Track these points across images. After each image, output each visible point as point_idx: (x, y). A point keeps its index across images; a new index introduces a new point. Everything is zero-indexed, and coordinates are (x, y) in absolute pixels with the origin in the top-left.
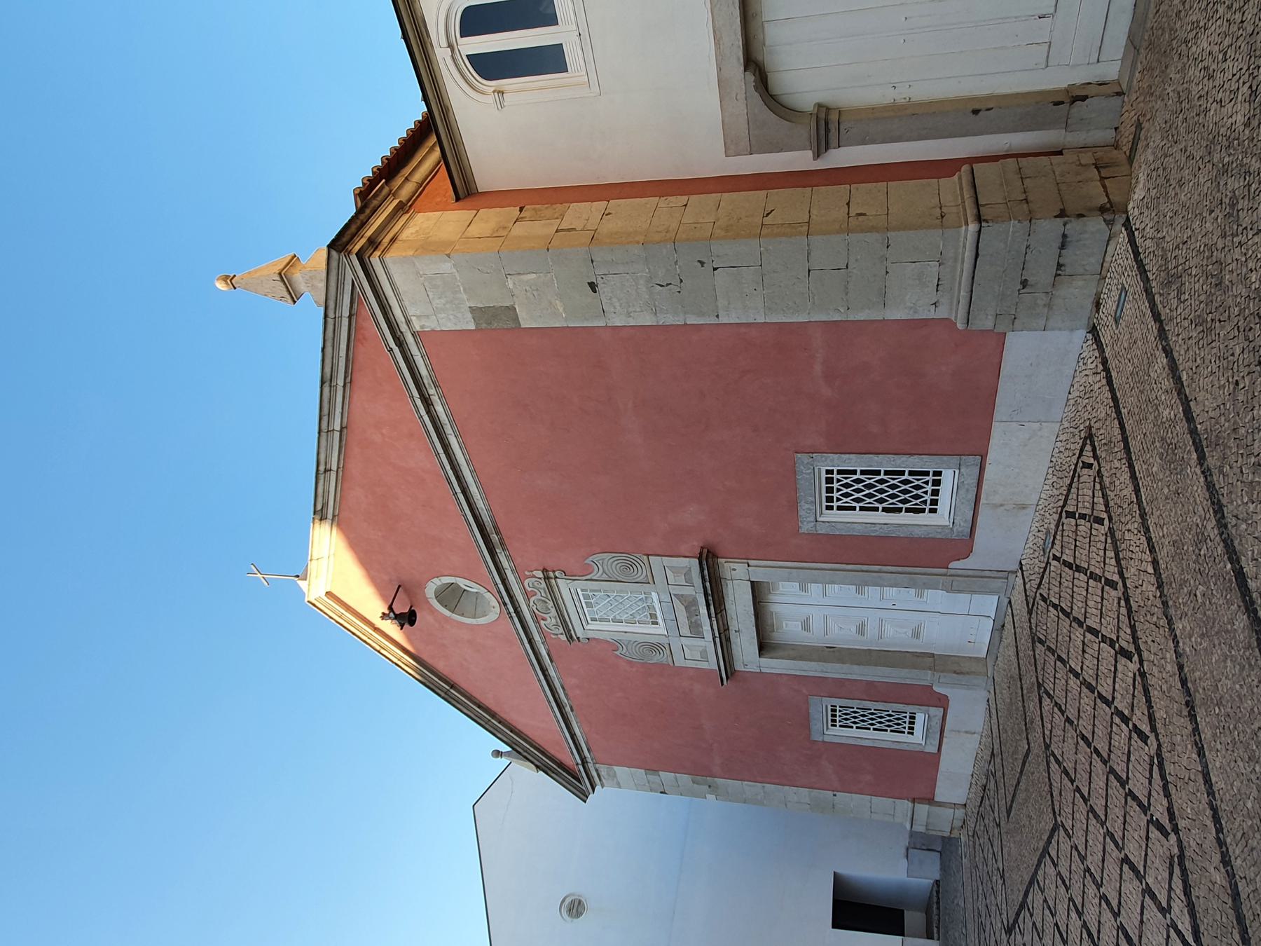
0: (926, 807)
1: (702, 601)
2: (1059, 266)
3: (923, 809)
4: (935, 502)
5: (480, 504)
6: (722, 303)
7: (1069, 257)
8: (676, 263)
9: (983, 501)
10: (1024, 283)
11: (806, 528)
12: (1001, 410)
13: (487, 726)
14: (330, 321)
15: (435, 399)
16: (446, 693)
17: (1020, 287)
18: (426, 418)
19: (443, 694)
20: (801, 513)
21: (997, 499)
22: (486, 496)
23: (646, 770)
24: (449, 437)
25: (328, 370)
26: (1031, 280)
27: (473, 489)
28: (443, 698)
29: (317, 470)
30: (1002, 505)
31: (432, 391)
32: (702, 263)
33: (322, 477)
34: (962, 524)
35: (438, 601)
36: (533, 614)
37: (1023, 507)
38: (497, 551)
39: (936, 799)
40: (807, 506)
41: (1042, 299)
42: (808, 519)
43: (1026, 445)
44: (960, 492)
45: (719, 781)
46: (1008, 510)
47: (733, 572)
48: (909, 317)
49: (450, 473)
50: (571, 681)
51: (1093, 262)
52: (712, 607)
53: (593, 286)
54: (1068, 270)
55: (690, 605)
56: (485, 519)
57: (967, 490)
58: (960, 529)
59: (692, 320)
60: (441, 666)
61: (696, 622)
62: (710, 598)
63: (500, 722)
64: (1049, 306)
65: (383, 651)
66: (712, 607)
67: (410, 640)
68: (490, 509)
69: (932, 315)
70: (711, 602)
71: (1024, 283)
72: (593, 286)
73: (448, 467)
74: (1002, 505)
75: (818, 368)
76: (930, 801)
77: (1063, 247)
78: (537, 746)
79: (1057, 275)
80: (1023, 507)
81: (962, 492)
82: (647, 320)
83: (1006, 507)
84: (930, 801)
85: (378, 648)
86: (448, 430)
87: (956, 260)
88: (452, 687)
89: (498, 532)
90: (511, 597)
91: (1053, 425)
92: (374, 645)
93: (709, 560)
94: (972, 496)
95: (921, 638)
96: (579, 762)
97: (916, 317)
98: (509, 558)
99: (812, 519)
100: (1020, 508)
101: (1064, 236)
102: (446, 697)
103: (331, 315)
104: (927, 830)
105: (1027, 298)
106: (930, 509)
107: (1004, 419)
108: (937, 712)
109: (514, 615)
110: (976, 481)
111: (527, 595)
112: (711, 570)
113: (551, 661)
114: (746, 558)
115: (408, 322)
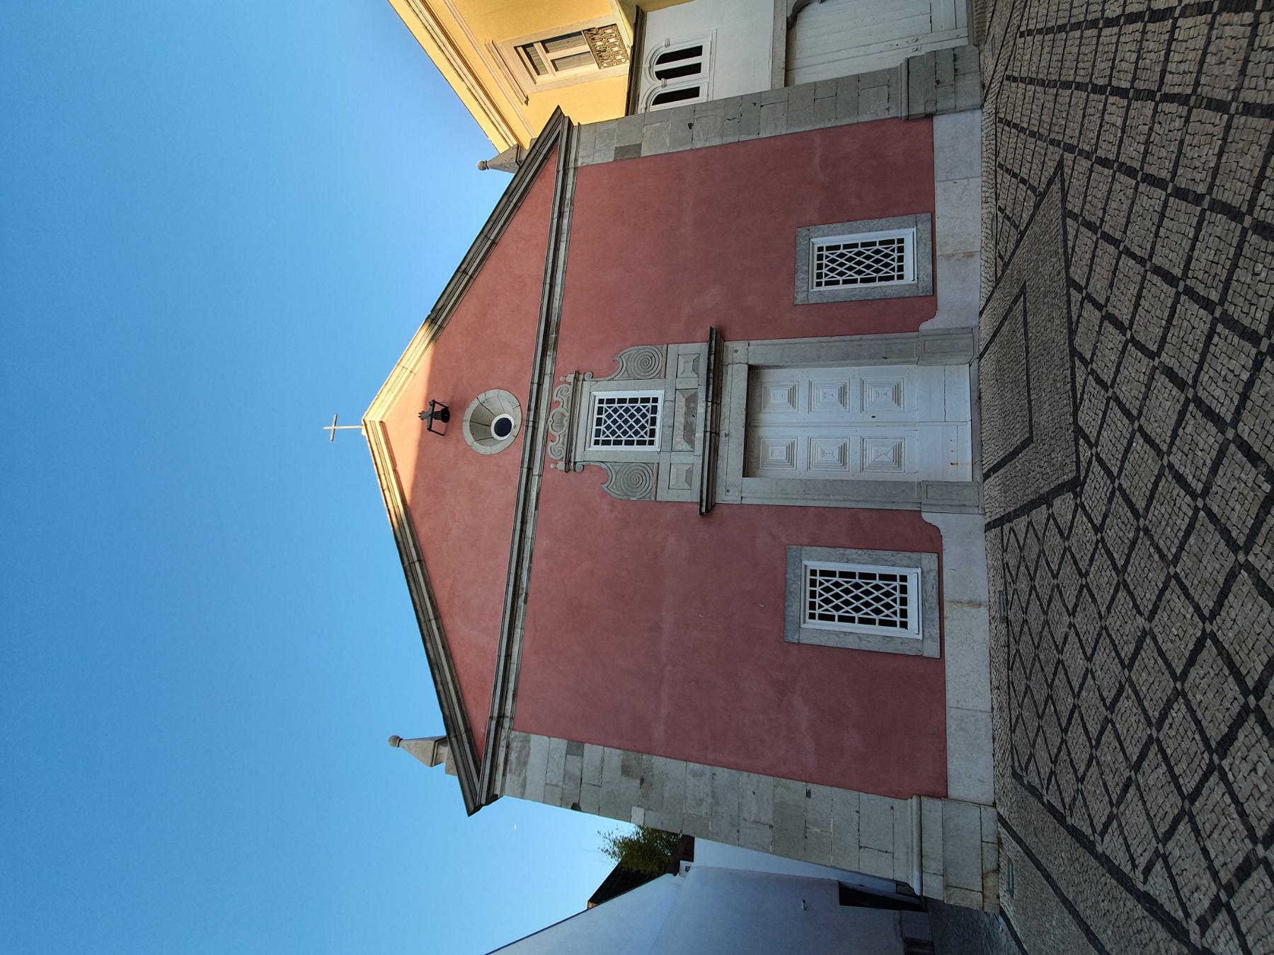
0: (939, 804)
1: (702, 395)
2: (956, 70)
3: (933, 808)
4: (901, 268)
5: (556, 304)
6: (763, 125)
7: (959, 64)
8: (741, 106)
9: (938, 253)
10: (938, 82)
11: (800, 298)
12: (939, 174)
13: (423, 625)
14: (534, 151)
15: (567, 214)
16: (410, 564)
17: (935, 84)
18: (555, 221)
19: (406, 563)
20: (798, 283)
21: (949, 250)
22: (562, 297)
23: (569, 740)
24: (501, 748)
25: (514, 185)
26: (941, 80)
27: (558, 289)
28: (404, 568)
29: (460, 267)
30: (953, 255)
31: (567, 209)
32: (755, 104)
33: (459, 274)
34: (925, 279)
35: (470, 426)
36: (546, 432)
37: (970, 255)
38: (549, 353)
39: (952, 793)
40: (803, 276)
41: (950, 90)
42: (803, 289)
43: (961, 199)
44: (920, 248)
45: (659, 762)
46: (959, 260)
47: (735, 354)
48: (873, 119)
49: (550, 265)
50: (544, 544)
51: (974, 66)
52: (711, 387)
53: (690, 126)
54: (962, 72)
55: (691, 400)
56: (553, 319)
57: (925, 244)
58: (924, 284)
59: (744, 138)
60: (424, 529)
61: (692, 423)
62: (711, 375)
63: (438, 629)
64: (955, 92)
65: (387, 493)
66: (711, 387)
67: (415, 486)
68: (560, 308)
69: (887, 116)
70: (711, 380)
71: (938, 82)
72: (690, 126)
73: (550, 261)
74: (953, 255)
75: (817, 161)
76: (942, 795)
77: (955, 60)
78: (458, 686)
79: (955, 75)
80: (970, 255)
81: (921, 246)
82: (716, 142)
83: (956, 257)
84: (942, 795)
85: (385, 487)
86: (564, 238)
87: (897, 83)
88: (419, 561)
89: (557, 332)
90: (537, 407)
91: (977, 179)
92: (384, 482)
93: (717, 341)
94: (929, 249)
95: (903, 467)
96: (496, 715)
97: (877, 118)
98: (554, 361)
99: (805, 289)
100: (968, 257)
101: (955, 55)
102: (408, 568)
103: (537, 148)
104: (947, 886)
105: (941, 90)
106: (898, 276)
107: (942, 179)
108: (929, 560)
109: (531, 424)
110: (930, 235)
111: (551, 406)
112: (718, 347)
113: (536, 508)
114: (748, 337)
115: (576, 160)
